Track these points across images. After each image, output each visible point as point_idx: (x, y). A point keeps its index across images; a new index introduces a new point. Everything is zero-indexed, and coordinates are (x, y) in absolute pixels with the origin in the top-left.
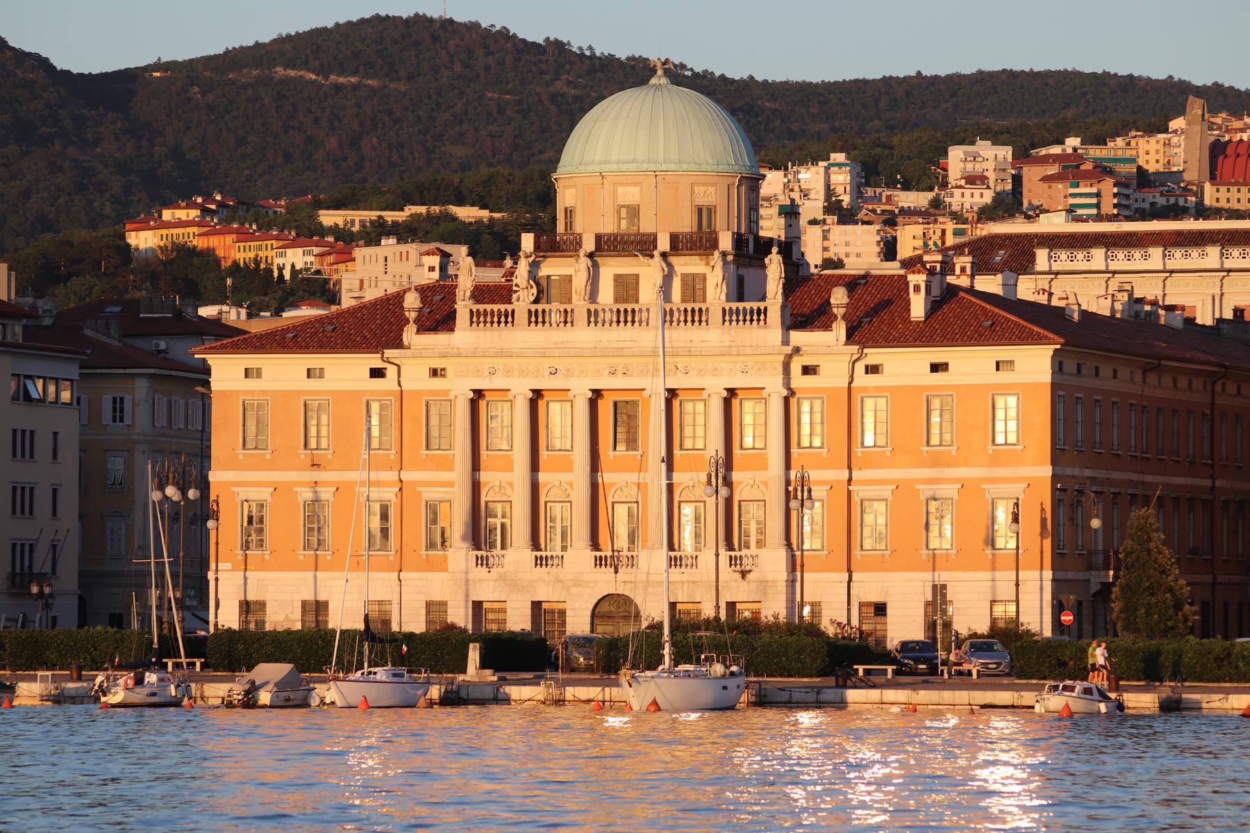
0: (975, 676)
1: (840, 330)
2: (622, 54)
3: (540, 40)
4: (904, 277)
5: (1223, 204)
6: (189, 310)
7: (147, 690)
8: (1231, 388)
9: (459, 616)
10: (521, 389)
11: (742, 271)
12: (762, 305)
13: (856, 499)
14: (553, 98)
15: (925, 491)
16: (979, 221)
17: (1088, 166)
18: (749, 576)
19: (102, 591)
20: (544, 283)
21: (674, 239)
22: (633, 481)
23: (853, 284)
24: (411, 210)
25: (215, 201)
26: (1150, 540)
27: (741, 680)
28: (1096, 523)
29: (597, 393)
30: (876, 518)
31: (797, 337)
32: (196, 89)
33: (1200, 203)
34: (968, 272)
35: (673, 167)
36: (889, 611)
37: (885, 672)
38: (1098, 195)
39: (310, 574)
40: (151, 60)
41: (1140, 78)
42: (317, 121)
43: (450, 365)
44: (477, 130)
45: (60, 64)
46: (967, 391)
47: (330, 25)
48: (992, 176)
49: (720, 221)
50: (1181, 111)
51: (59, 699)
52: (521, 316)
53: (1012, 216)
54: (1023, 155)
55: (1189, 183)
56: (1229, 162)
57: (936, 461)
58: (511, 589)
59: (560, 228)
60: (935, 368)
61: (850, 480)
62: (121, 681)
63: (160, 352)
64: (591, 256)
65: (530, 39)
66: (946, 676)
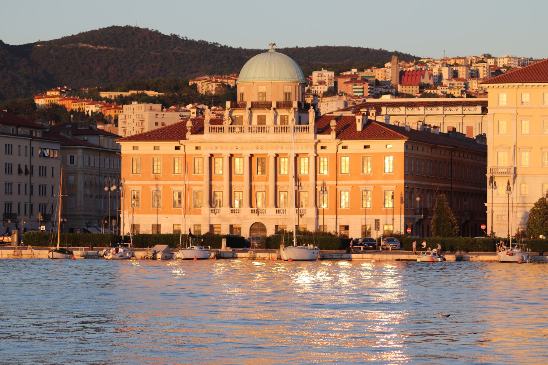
0: (390, 249)
1: (333, 134)
2: (197, 40)
3: (169, 35)
4: (354, 117)
5: (404, 92)
6: (94, 127)
7: (120, 255)
8: (457, 154)
10: (226, 153)
11: (300, 114)
12: (307, 126)
13: (339, 191)
14: (174, 54)
15: (362, 188)
16: (323, 96)
17: (359, 79)
18: (303, 217)
19: (88, 221)
20: (234, 118)
21: (278, 104)
22: (264, 185)
23: (337, 119)
24: (131, 92)
25: (64, 89)
26: (444, 204)
27: (317, 251)
28: (418, 199)
29: (252, 155)
30: (345, 199)
31: (319, 137)
32: (52, 50)
33: (397, 91)
34: (374, 115)
35: (277, 79)
36: (350, 228)
37: (360, 248)
38: (363, 88)
39: (155, 216)
40: (36, 41)
41: (370, 49)
42: (93, 61)
43: (202, 146)
44: (148, 65)
45: (6, 42)
46: (164, 156)
47: (97, 29)
48: (327, 81)
49: (293, 98)
50: (389, 60)
51: (86, 257)
52: (226, 129)
53: (334, 95)
54: (337, 75)
55: (393, 85)
56: (406, 77)
57: (367, 178)
58: (222, 222)
59: (239, 99)
60: (365, 147)
61: (337, 185)
62: (111, 251)
63: (85, 140)
64: (250, 109)
65: (165, 34)
66: (381, 250)
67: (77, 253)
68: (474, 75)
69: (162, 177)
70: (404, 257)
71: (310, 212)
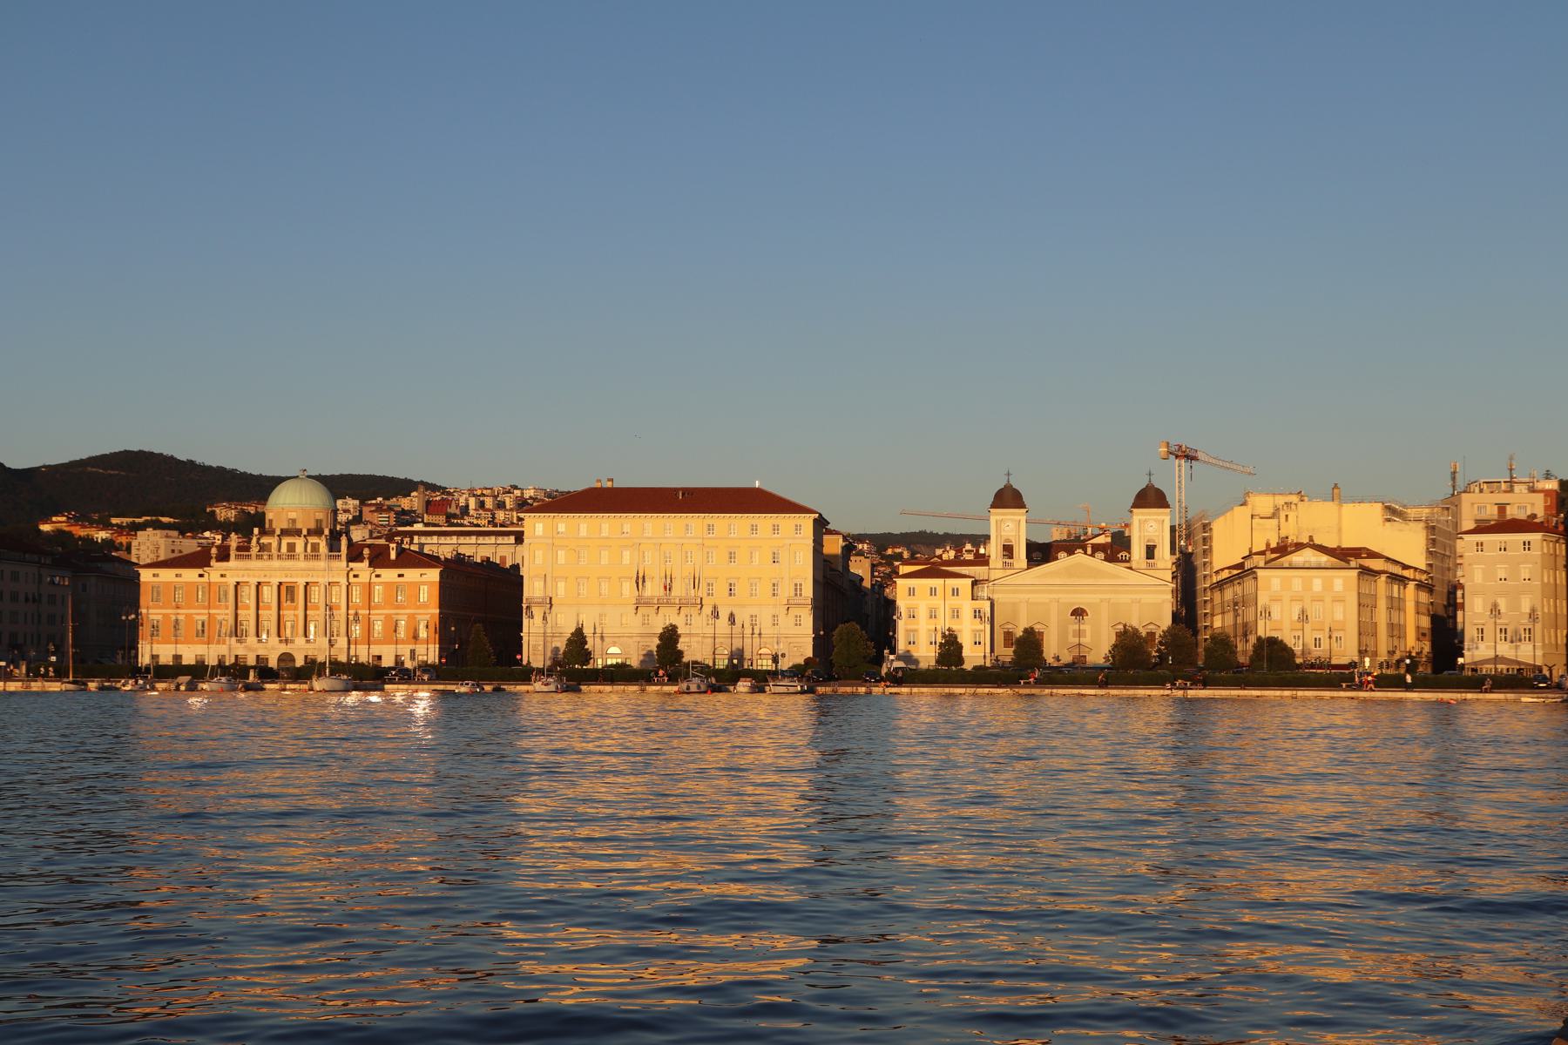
1: (366, 563)
9: (251, 661)
10: (254, 581)
22: (293, 614)
23: (369, 546)
30: (378, 627)
31: (352, 565)
46: (410, 584)
54: (362, 503)
57: (398, 607)
58: (248, 650)
67: (92, 686)
68: (501, 505)
69: (187, 606)
70: (441, 687)
71: (342, 642)
